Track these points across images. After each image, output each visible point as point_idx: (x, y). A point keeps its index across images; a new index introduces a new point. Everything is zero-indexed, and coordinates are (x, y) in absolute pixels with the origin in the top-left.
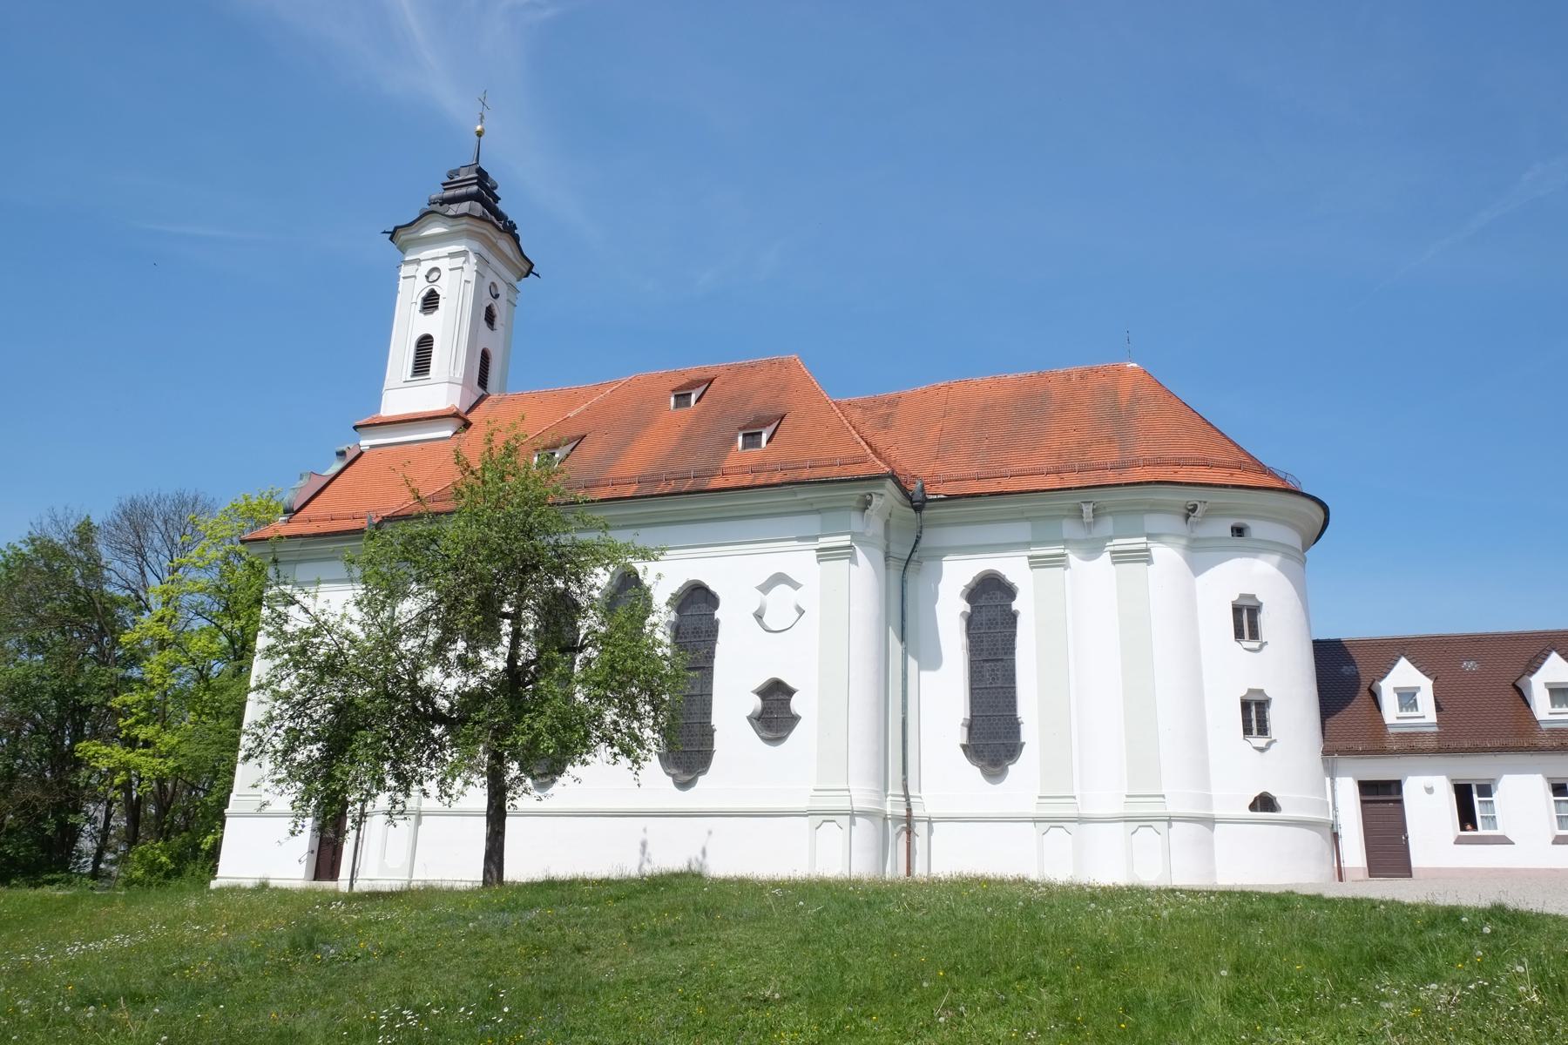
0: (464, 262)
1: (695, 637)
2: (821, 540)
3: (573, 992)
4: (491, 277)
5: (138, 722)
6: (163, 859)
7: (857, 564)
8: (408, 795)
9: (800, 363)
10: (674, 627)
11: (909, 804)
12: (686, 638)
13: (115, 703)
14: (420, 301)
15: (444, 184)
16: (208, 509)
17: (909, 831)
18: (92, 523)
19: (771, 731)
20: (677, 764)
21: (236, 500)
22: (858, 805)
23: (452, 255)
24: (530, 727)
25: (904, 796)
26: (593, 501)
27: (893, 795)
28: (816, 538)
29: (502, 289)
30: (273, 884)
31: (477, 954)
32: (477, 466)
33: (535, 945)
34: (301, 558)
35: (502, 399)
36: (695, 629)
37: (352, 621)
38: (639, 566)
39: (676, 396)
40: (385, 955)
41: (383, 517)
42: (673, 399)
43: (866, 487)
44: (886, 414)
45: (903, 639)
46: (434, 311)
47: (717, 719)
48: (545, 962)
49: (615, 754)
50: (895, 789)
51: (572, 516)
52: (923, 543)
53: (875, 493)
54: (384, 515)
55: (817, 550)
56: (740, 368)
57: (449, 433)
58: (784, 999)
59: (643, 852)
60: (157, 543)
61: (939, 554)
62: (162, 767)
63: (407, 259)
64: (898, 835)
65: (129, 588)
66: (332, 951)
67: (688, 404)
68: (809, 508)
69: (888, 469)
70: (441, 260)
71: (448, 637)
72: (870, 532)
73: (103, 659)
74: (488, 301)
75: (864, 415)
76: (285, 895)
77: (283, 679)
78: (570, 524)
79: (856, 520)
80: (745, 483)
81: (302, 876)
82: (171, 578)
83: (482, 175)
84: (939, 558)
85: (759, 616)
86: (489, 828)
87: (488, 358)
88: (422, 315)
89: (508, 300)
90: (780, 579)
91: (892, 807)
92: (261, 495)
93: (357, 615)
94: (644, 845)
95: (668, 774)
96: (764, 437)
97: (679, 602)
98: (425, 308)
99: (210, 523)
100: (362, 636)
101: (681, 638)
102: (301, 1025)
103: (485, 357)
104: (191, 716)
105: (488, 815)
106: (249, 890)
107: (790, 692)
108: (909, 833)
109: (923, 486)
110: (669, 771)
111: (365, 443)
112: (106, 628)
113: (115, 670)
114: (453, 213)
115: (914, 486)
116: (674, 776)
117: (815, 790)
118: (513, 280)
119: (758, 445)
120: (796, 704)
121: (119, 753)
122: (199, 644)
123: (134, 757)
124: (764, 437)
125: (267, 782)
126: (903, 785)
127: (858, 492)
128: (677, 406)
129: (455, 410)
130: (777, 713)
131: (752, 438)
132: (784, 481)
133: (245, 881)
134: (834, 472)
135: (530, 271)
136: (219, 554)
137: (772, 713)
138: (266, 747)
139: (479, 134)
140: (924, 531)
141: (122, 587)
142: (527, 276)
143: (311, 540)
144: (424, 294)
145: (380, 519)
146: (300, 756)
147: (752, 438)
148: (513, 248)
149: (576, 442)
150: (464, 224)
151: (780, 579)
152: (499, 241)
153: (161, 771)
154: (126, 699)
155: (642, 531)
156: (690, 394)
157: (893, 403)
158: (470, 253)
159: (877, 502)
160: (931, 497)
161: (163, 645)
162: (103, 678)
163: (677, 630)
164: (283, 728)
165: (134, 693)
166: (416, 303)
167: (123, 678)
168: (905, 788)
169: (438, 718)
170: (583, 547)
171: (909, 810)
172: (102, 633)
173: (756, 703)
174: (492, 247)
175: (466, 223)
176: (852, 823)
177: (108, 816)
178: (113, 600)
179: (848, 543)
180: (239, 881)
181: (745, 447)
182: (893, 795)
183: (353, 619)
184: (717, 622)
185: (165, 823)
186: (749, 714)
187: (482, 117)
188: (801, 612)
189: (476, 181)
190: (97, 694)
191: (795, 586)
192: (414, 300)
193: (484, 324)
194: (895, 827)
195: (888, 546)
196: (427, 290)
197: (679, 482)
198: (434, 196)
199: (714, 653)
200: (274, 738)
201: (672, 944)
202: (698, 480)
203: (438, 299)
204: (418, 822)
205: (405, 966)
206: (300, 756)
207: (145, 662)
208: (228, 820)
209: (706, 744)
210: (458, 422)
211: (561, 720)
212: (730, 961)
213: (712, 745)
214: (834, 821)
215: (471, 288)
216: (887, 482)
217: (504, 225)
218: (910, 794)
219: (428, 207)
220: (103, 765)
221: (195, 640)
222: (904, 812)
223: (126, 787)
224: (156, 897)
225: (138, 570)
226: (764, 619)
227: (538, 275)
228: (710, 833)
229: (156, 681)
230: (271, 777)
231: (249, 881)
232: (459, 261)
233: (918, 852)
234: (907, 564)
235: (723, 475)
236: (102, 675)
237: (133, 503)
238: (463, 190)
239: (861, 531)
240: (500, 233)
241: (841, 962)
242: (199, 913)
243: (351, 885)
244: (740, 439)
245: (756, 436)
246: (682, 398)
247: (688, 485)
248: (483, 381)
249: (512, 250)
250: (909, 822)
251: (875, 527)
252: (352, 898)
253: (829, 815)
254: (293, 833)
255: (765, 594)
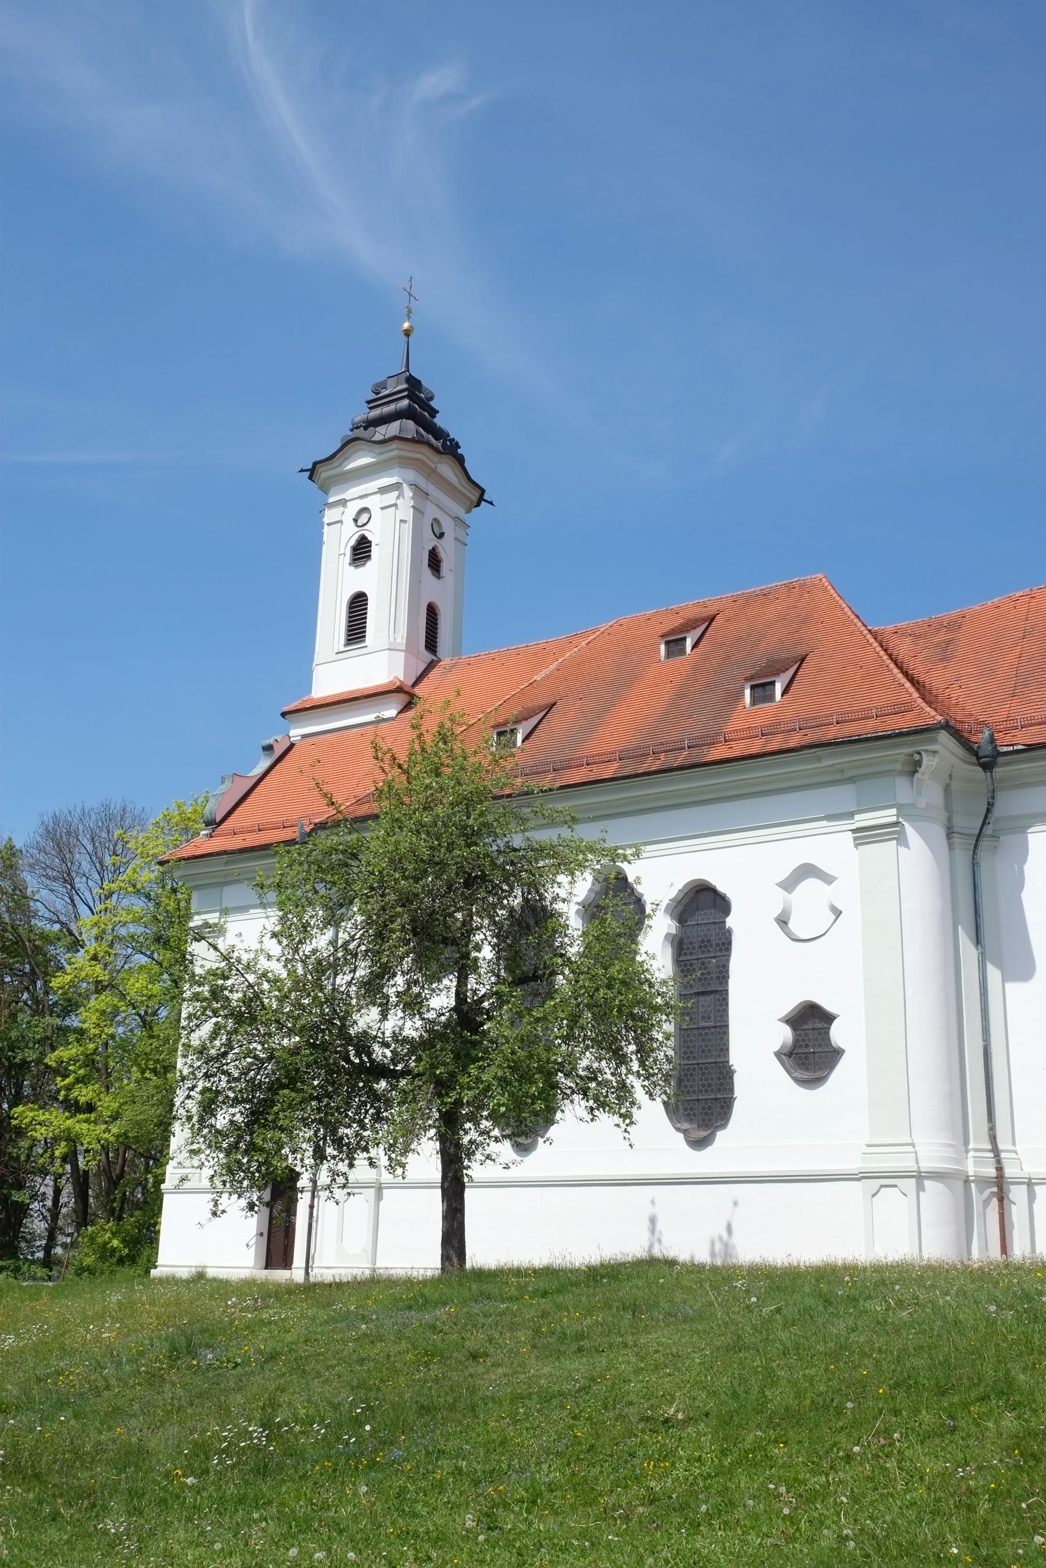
0: (398, 498)
1: (703, 952)
2: (857, 817)
3: (452, 1408)
4: (432, 512)
5: (78, 1081)
6: (115, 1243)
7: (907, 846)
8: (351, 1166)
9: (827, 584)
10: (677, 940)
11: (999, 1162)
12: (691, 954)
13: (51, 1059)
14: (348, 552)
15: (369, 402)
16: (139, 821)
17: (1002, 1197)
18: (14, 847)
19: (807, 1069)
20: (689, 1118)
21: (167, 809)
22: (927, 1164)
23: (383, 490)
24: (478, 1080)
25: (992, 1151)
26: (551, 790)
27: (976, 1150)
28: (851, 815)
29: (448, 526)
30: (211, 1273)
31: (362, 1361)
32: (402, 758)
33: (426, 1351)
34: (227, 879)
35: (455, 665)
36: (703, 941)
37: (269, 957)
38: (624, 866)
39: (667, 643)
40: (267, 1361)
41: (316, 824)
42: (663, 647)
43: (913, 744)
44: (944, 641)
45: (978, 941)
46: (366, 562)
47: (735, 1059)
48: (435, 1370)
49: (592, 1109)
50: (979, 1141)
51: (529, 810)
52: (997, 812)
53: (926, 751)
54: (317, 821)
55: (854, 831)
56: (749, 599)
57: (391, 713)
58: (689, 1420)
59: (653, 1231)
60: (86, 866)
61: (1021, 825)
62: (106, 1135)
63: (331, 500)
64: (986, 1203)
65: (59, 922)
66: (210, 1356)
67: (683, 652)
68: (839, 777)
69: (939, 718)
70: (370, 497)
71: (382, 973)
72: (922, 803)
73: (39, 1008)
74: (430, 542)
75: (916, 645)
76: (222, 1288)
77: (193, 1031)
78: (528, 820)
79: (902, 789)
80: (754, 750)
81: (252, 1264)
82: (103, 907)
83: (414, 385)
84: (1023, 830)
85: (783, 921)
86: (445, 1204)
87: (436, 615)
88: (352, 568)
89: (456, 539)
90: (806, 871)
91: (976, 1164)
92: (196, 801)
93: (274, 948)
94: (653, 1221)
95: (678, 1130)
96: (779, 688)
97: (680, 908)
98: (355, 560)
99: (141, 840)
100: (284, 974)
101: (685, 954)
102: (153, 1443)
103: (432, 612)
104: (136, 1074)
105: (442, 1187)
106: (184, 1281)
107: (828, 1018)
108: (1001, 1200)
109: (992, 736)
110: (679, 1125)
111: (296, 733)
112: (37, 970)
113: (48, 1019)
114: (381, 438)
115: (981, 736)
116: (685, 1132)
117: (868, 1146)
118: (460, 512)
119: (771, 698)
120: (838, 1034)
121: (57, 1119)
122: (137, 985)
123: (78, 1125)
124: (779, 688)
125: (184, 1152)
126: (990, 1135)
127: (902, 751)
128: (669, 655)
129: (398, 684)
130: (814, 1046)
131: (762, 690)
132: (803, 743)
133: (179, 1269)
134: (869, 728)
135: (481, 499)
136: (152, 876)
137: (807, 1046)
138: (179, 1111)
139: (407, 333)
140: (999, 795)
141: (50, 920)
142: (478, 505)
143: (238, 856)
144: (353, 542)
145: (312, 826)
146: (221, 1120)
147: (762, 690)
148: (458, 473)
149: (546, 711)
150: (394, 450)
151: (806, 871)
152: (439, 466)
153: (106, 1140)
154: (61, 1054)
155: (612, 824)
156: (684, 639)
157: (954, 625)
158: (405, 485)
159: (928, 762)
160: (1005, 749)
161: (100, 987)
162: (37, 1030)
163: (680, 946)
164: (197, 1090)
165: (70, 1047)
166: (345, 554)
167: (60, 1028)
168: (993, 1139)
169: (380, 1071)
170: (540, 851)
171: (1000, 1169)
172: (33, 976)
173: (785, 1035)
174: (432, 474)
175: (398, 449)
176: (920, 1188)
177: (57, 1192)
178: (44, 937)
179: (894, 819)
180: (174, 1270)
181: (754, 702)
182: (976, 1150)
183: (271, 954)
184: (729, 932)
185: (115, 1200)
186: (777, 1049)
187: (410, 311)
188: (837, 913)
189: (406, 393)
190: (33, 1048)
191: (828, 879)
192: (342, 552)
193: (427, 572)
194: (981, 1192)
195: (950, 819)
196: (356, 537)
197: (670, 755)
198: (357, 419)
199: (727, 971)
200: (186, 1101)
201: (580, 1350)
202: (695, 751)
203: (370, 546)
204: (379, 1197)
205: (284, 1374)
206: (221, 1120)
207: (82, 1009)
208: (165, 1196)
209: (725, 1089)
210: (403, 699)
211: (513, 1069)
212: (638, 1371)
213: (732, 1090)
214: (895, 1186)
215: (408, 528)
216: (940, 735)
217: (444, 445)
218: (1001, 1147)
219: (350, 433)
220: (40, 1133)
221: (132, 981)
222: (992, 1172)
223: (70, 1157)
224: (83, 1290)
225: (69, 901)
226: (790, 925)
227: (491, 503)
228: (735, 1203)
229: (93, 1031)
230: (189, 1148)
231: (185, 1269)
232: (391, 497)
233: (1016, 1225)
234: (977, 840)
235: (726, 741)
236: (36, 1026)
237: (56, 819)
238: (392, 407)
239: (910, 801)
240: (439, 456)
241: (770, 1372)
242: (120, 1309)
243: (307, 1273)
244: (747, 692)
245: (767, 688)
246: (675, 645)
247: (681, 758)
248: (431, 644)
249: (456, 476)
250: (1000, 1186)
251: (931, 794)
252: (310, 1289)
253: (888, 1178)
254: (214, 1214)
255: (790, 893)
